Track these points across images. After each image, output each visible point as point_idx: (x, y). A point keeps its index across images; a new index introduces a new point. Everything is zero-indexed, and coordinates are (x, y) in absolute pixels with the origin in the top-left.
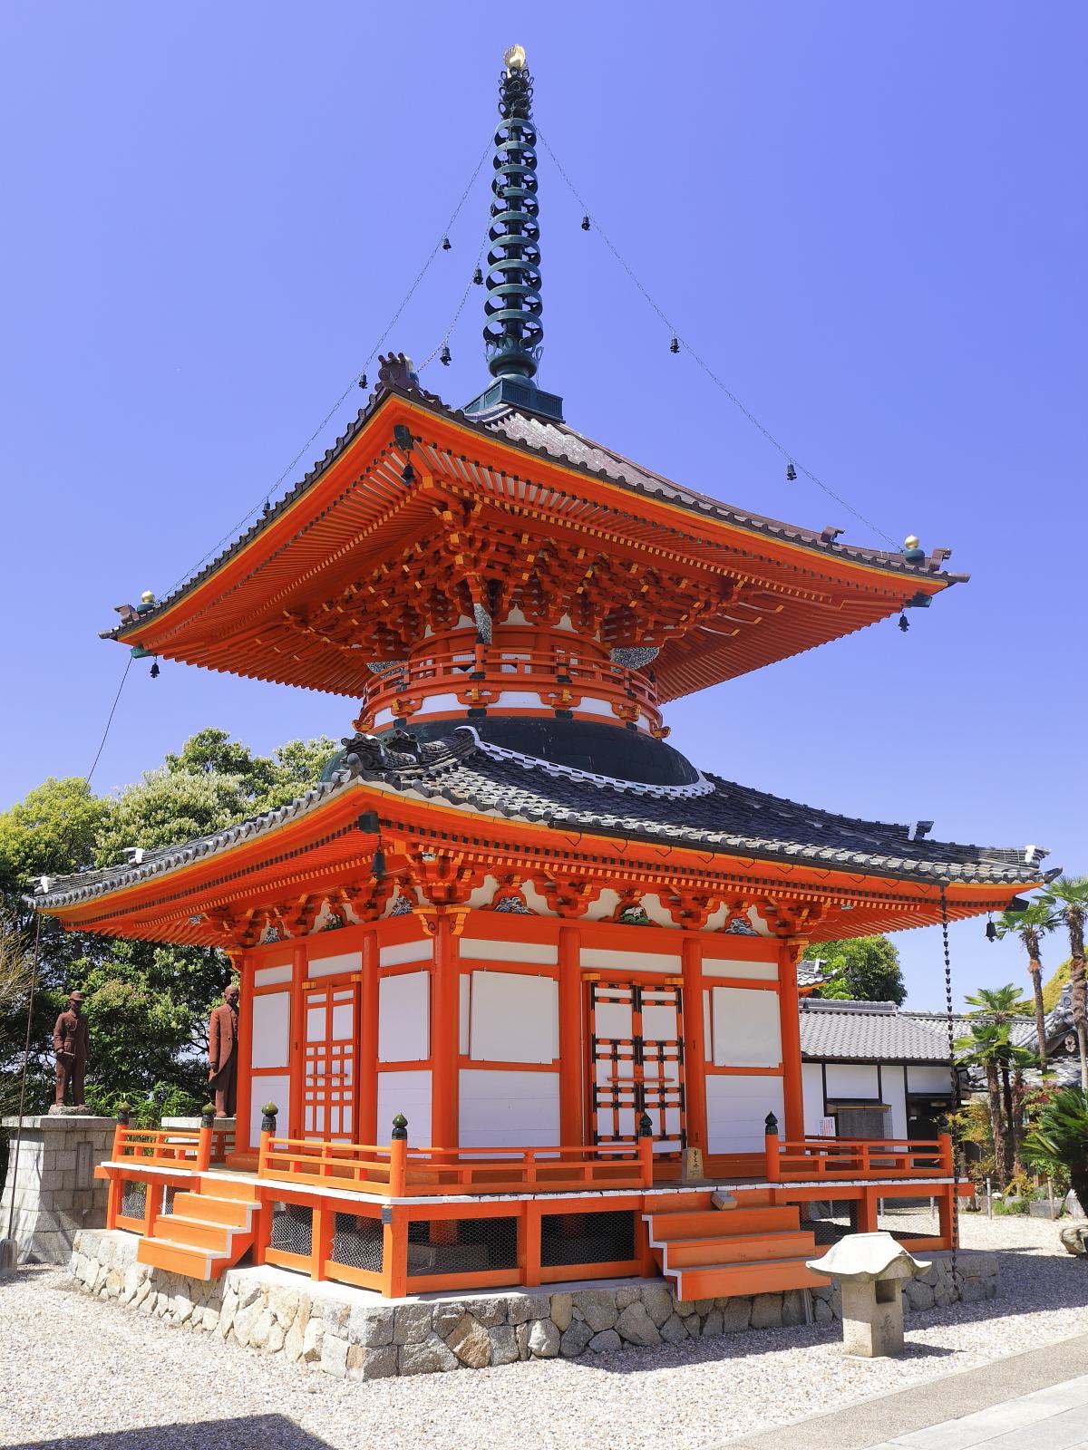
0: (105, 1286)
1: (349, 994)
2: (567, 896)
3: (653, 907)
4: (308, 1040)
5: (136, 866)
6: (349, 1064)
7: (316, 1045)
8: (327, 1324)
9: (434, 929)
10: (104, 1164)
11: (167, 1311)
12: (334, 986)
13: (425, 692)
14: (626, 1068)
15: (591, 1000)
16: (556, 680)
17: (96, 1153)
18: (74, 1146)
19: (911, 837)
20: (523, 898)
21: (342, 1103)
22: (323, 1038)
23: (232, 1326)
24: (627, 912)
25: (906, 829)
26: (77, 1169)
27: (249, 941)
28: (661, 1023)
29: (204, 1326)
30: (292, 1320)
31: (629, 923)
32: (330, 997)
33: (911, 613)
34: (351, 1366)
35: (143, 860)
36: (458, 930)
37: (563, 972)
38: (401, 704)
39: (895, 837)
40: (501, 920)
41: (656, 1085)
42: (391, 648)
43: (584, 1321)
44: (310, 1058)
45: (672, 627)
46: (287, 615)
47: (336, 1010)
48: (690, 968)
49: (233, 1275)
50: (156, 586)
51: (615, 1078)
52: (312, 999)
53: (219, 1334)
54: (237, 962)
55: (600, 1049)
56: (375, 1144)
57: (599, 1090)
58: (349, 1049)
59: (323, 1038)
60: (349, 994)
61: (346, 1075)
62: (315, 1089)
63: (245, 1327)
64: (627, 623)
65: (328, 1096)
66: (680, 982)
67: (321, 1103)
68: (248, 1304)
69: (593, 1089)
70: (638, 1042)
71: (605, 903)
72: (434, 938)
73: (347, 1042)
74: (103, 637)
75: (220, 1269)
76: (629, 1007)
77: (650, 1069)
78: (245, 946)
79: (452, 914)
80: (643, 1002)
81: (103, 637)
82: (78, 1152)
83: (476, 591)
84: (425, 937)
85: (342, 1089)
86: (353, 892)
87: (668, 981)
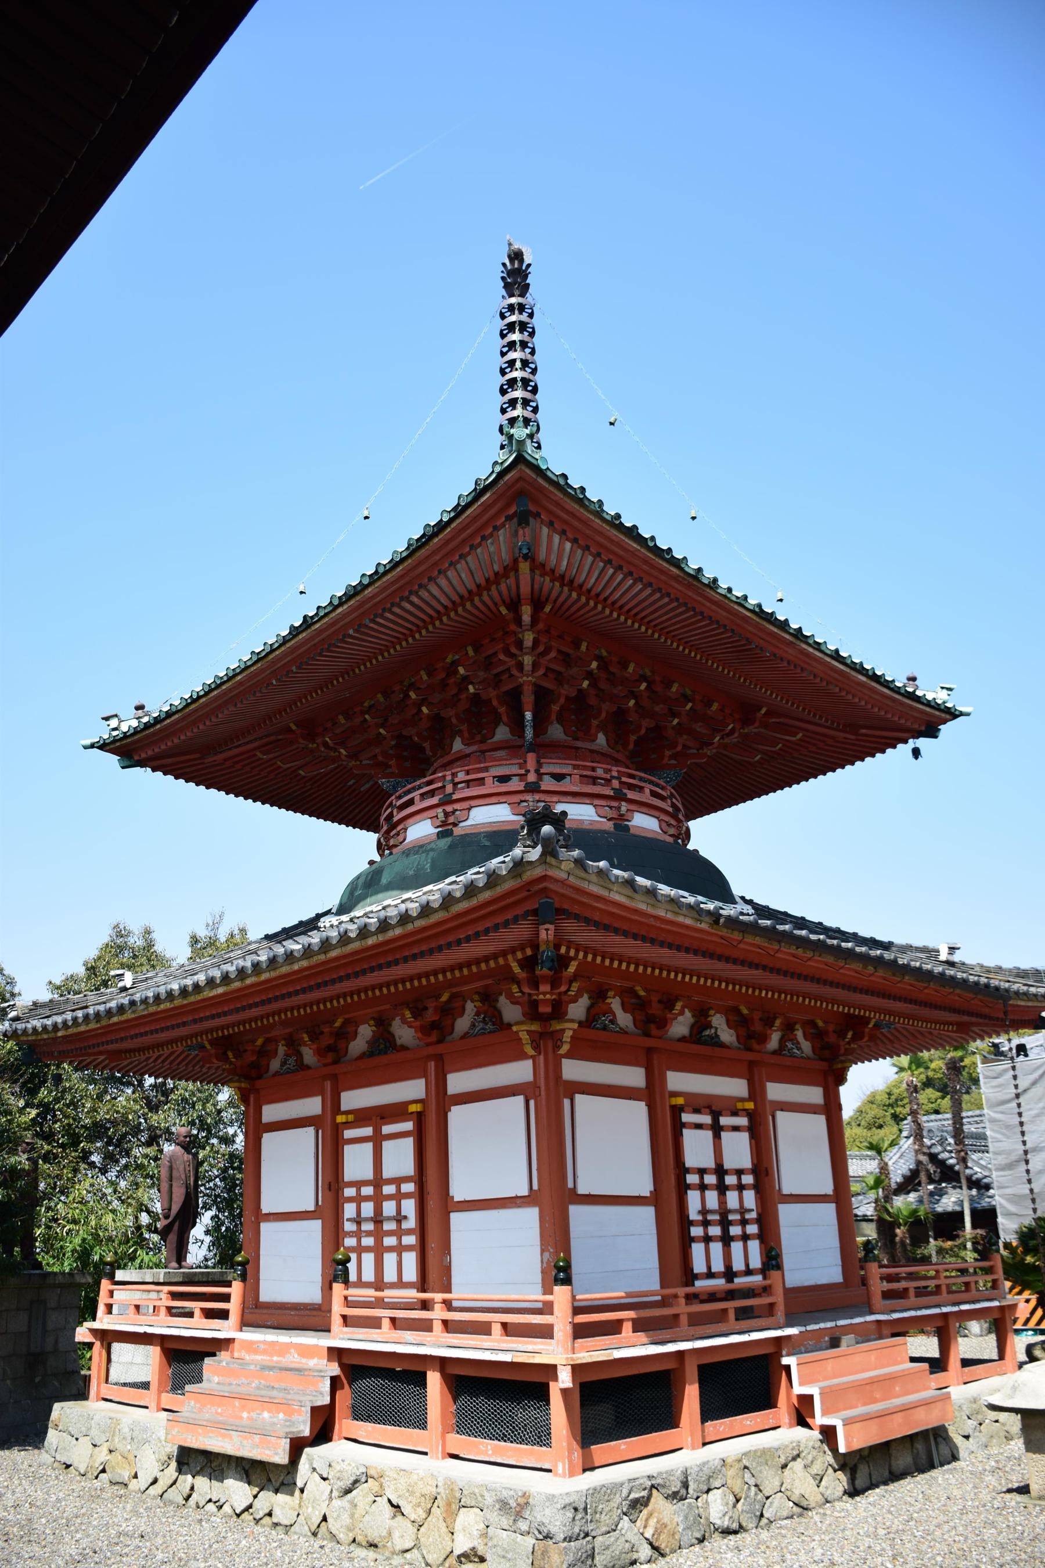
0: (103, 1471)
1: (408, 1126)
2: (651, 1018)
4: (346, 1180)
5: (124, 989)
6: (409, 1207)
7: (358, 1184)
8: (493, 1516)
9: (536, 1047)
11: (210, 1501)
12: (382, 1118)
13: (473, 803)
14: (712, 1199)
15: (678, 1127)
16: (612, 793)
21: (400, 1249)
23: (325, 1519)
28: (738, 1150)
29: (275, 1520)
30: (429, 1512)
32: (377, 1131)
33: (922, 743)
35: (134, 983)
36: (565, 1048)
37: (652, 1094)
38: (446, 814)
40: (596, 1044)
41: (738, 1217)
42: (407, 764)
44: (350, 1200)
45: (695, 751)
46: (294, 727)
47: (387, 1146)
48: (756, 1092)
51: (704, 1211)
52: (348, 1134)
53: (302, 1528)
56: (450, 1292)
57: (692, 1223)
58: (409, 1187)
59: (369, 1175)
60: (408, 1126)
61: (405, 1217)
65: (379, 1241)
66: (750, 1105)
67: (368, 1249)
68: (348, 1491)
69: (686, 1223)
71: (681, 1026)
73: (406, 1179)
75: (297, 1446)
76: (709, 1134)
77: (732, 1199)
79: (557, 1031)
83: (528, 698)
84: (523, 1056)
85: (399, 1233)
86: (314, 1037)
87: (740, 1106)
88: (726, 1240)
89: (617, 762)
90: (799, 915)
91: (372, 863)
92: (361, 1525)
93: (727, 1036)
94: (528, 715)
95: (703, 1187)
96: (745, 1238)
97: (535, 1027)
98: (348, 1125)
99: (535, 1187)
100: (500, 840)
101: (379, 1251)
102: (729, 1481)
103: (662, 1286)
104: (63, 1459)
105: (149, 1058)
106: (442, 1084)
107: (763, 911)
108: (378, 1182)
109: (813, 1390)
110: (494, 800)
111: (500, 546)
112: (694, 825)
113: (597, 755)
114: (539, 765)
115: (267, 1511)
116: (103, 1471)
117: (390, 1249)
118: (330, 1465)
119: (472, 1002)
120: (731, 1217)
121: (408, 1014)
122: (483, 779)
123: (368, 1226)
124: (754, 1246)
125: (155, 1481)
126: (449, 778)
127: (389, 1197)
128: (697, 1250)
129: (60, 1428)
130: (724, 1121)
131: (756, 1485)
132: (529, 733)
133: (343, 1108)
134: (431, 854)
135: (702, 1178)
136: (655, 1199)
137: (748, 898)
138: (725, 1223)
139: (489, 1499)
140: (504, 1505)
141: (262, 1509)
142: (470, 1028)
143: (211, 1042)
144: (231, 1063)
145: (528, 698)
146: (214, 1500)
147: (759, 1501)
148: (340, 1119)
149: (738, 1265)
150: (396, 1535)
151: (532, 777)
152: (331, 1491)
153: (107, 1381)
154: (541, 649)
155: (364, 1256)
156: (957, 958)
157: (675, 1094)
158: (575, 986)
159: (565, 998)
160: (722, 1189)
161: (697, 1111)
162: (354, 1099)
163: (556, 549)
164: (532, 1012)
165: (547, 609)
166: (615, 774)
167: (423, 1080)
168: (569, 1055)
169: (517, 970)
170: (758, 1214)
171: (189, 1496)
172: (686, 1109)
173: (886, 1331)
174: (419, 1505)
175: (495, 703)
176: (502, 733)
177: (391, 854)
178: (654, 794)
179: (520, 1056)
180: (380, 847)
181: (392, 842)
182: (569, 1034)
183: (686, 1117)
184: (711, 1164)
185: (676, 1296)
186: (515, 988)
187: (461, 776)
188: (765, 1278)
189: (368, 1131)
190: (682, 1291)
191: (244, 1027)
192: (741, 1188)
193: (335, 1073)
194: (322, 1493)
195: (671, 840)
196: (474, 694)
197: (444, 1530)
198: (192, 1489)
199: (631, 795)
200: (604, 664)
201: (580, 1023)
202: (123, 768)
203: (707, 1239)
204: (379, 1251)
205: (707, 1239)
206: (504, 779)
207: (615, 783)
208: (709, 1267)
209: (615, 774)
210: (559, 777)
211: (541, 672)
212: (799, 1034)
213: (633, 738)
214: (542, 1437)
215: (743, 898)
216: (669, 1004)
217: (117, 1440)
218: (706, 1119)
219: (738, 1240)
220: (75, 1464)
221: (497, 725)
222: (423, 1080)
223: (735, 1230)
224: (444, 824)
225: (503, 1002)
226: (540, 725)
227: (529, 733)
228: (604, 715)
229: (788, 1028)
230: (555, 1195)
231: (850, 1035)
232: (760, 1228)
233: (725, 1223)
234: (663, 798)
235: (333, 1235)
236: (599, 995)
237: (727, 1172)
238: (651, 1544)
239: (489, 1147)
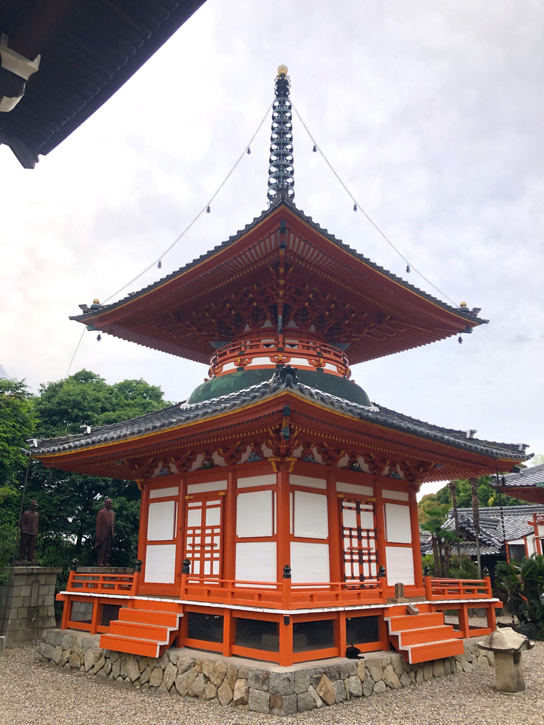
0: (68, 662)
1: (219, 502)
3: (362, 463)
6: (217, 540)
7: (194, 529)
8: (252, 683)
9: (278, 469)
10: (61, 593)
11: (120, 675)
12: (207, 498)
14: (355, 542)
15: (341, 508)
16: (316, 354)
17: (41, 587)
18: (30, 583)
19: (468, 436)
20: (313, 455)
21: (212, 559)
22: (199, 525)
23: (174, 684)
24: (354, 465)
25: (465, 433)
26: (31, 596)
27: (148, 475)
29: (150, 684)
30: (223, 681)
31: (354, 470)
32: (204, 504)
33: (463, 335)
34: (274, 708)
36: (291, 469)
39: (460, 436)
40: (305, 467)
41: (367, 552)
42: (223, 335)
43: (371, 676)
44: (190, 535)
45: (355, 335)
46: (171, 315)
47: (208, 511)
49: (173, 654)
50: (112, 294)
51: (351, 548)
52: (190, 505)
54: (141, 485)
55: (346, 532)
57: (345, 553)
58: (217, 531)
59: (199, 525)
61: (216, 545)
62: (193, 552)
63: (184, 684)
64: (337, 331)
66: (374, 500)
67: (197, 559)
68: (186, 671)
69: (343, 553)
70: (359, 530)
71: (344, 461)
72: (277, 473)
73: (198, 528)
74: (71, 318)
76: (355, 512)
78: (146, 478)
80: (361, 510)
81: (71, 318)
82: (32, 586)
83: (280, 309)
84: (273, 473)
85: (212, 552)
87: (369, 500)
88: (361, 561)
89: (318, 339)
90: (400, 413)
91: (206, 380)
92: (191, 687)
93: (365, 467)
94: (280, 317)
95: (351, 537)
96: (370, 561)
97: (278, 459)
98: (191, 501)
99: (275, 533)
100: (264, 373)
101: (202, 560)
102: (359, 673)
103: (331, 581)
104: (48, 656)
105: (97, 467)
106: (235, 483)
107: (384, 410)
108: (203, 527)
109: (398, 633)
110: (264, 354)
111: (271, 242)
112: (352, 368)
113: (311, 336)
114: (284, 339)
115: (147, 680)
116: (68, 662)
117: (208, 559)
118: (178, 659)
119: (250, 446)
120: (363, 552)
121: (221, 450)
122: (259, 345)
123: (198, 548)
124: (374, 565)
125: (93, 667)
126: (243, 344)
127: (208, 535)
128: (348, 565)
129: (47, 642)
130: (362, 506)
131: (371, 676)
132: (280, 325)
133: (189, 493)
134: (234, 378)
135: (351, 533)
136: (328, 541)
137: (377, 403)
138: (361, 554)
139: (251, 675)
140: (257, 678)
141: (145, 679)
142: (249, 458)
143: (127, 461)
144: (136, 470)
145: (280, 309)
146: (121, 675)
147: (371, 683)
148: (187, 498)
149: (366, 574)
150: (208, 691)
151: (281, 345)
152: (178, 671)
153: (70, 620)
154: (287, 287)
155: (195, 562)
156: (475, 436)
157: (340, 493)
158: (297, 442)
159: (292, 447)
160: (360, 538)
161: (349, 501)
162: (193, 489)
163: (295, 243)
164: (277, 453)
165: (291, 269)
166: (318, 345)
167: (226, 481)
168: (293, 473)
169: (271, 433)
170: (376, 550)
171: (110, 673)
172: (344, 500)
173: (433, 609)
174: (218, 677)
175: (265, 310)
176: (268, 324)
177: (215, 377)
178: (335, 354)
179: (271, 472)
180: (210, 373)
181: (217, 371)
182: (293, 463)
183: (344, 504)
184: (355, 526)
185: (337, 585)
186: (270, 442)
187: (248, 343)
188: (378, 580)
189: (200, 504)
190: (340, 583)
191: (168, 449)
192: (368, 538)
193: (187, 477)
194: (174, 672)
195: (342, 376)
196: (256, 306)
197: (230, 689)
198: (111, 670)
199: (325, 355)
200: (315, 295)
201: (298, 458)
202: (89, 330)
203: (352, 561)
204: (202, 560)
205: (352, 561)
206: (268, 345)
207: (318, 350)
208: (352, 574)
209: (318, 345)
210: (292, 345)
211: (287, 297)
212: (398, 468)
213: (327, 328)
214: (275, 647)
215: (374, 404)
216: (338, 451)
217: (75, 647)
218: (354, 505)
219: (366, 562)
220: (54, 659)
221: (265, 320)
222: (226, 481)
223: (365, 558)
224: (240, 364)
225: (264, 447)
226: (285, 322)
227: (280, 325)
228: (314, 318)
229: (393, 465)
230: (283, 537)
231: (422, 469)
232: (377, 557)
233: (361, 554)
234: (340, 357)
235: (181, 551)
236: (307, 446)
237: (362, 530)
238: (322, 699)
239: (255, 513)
